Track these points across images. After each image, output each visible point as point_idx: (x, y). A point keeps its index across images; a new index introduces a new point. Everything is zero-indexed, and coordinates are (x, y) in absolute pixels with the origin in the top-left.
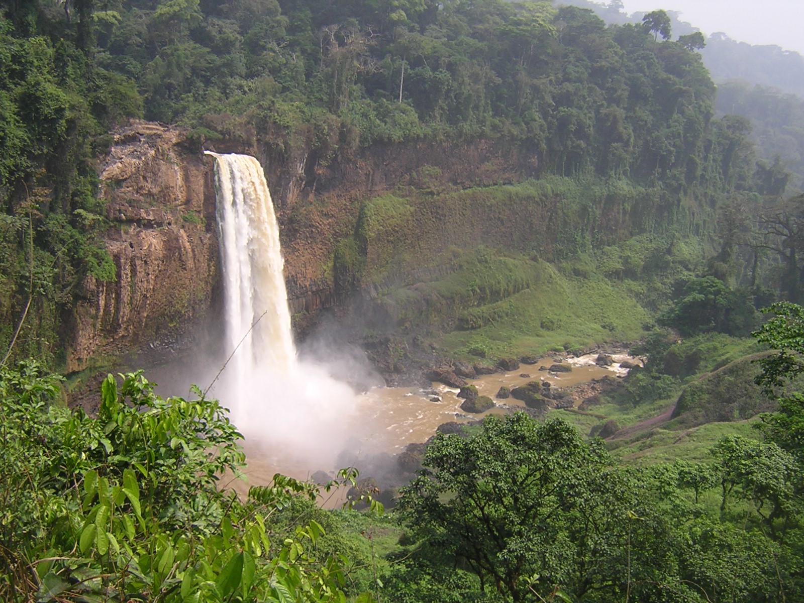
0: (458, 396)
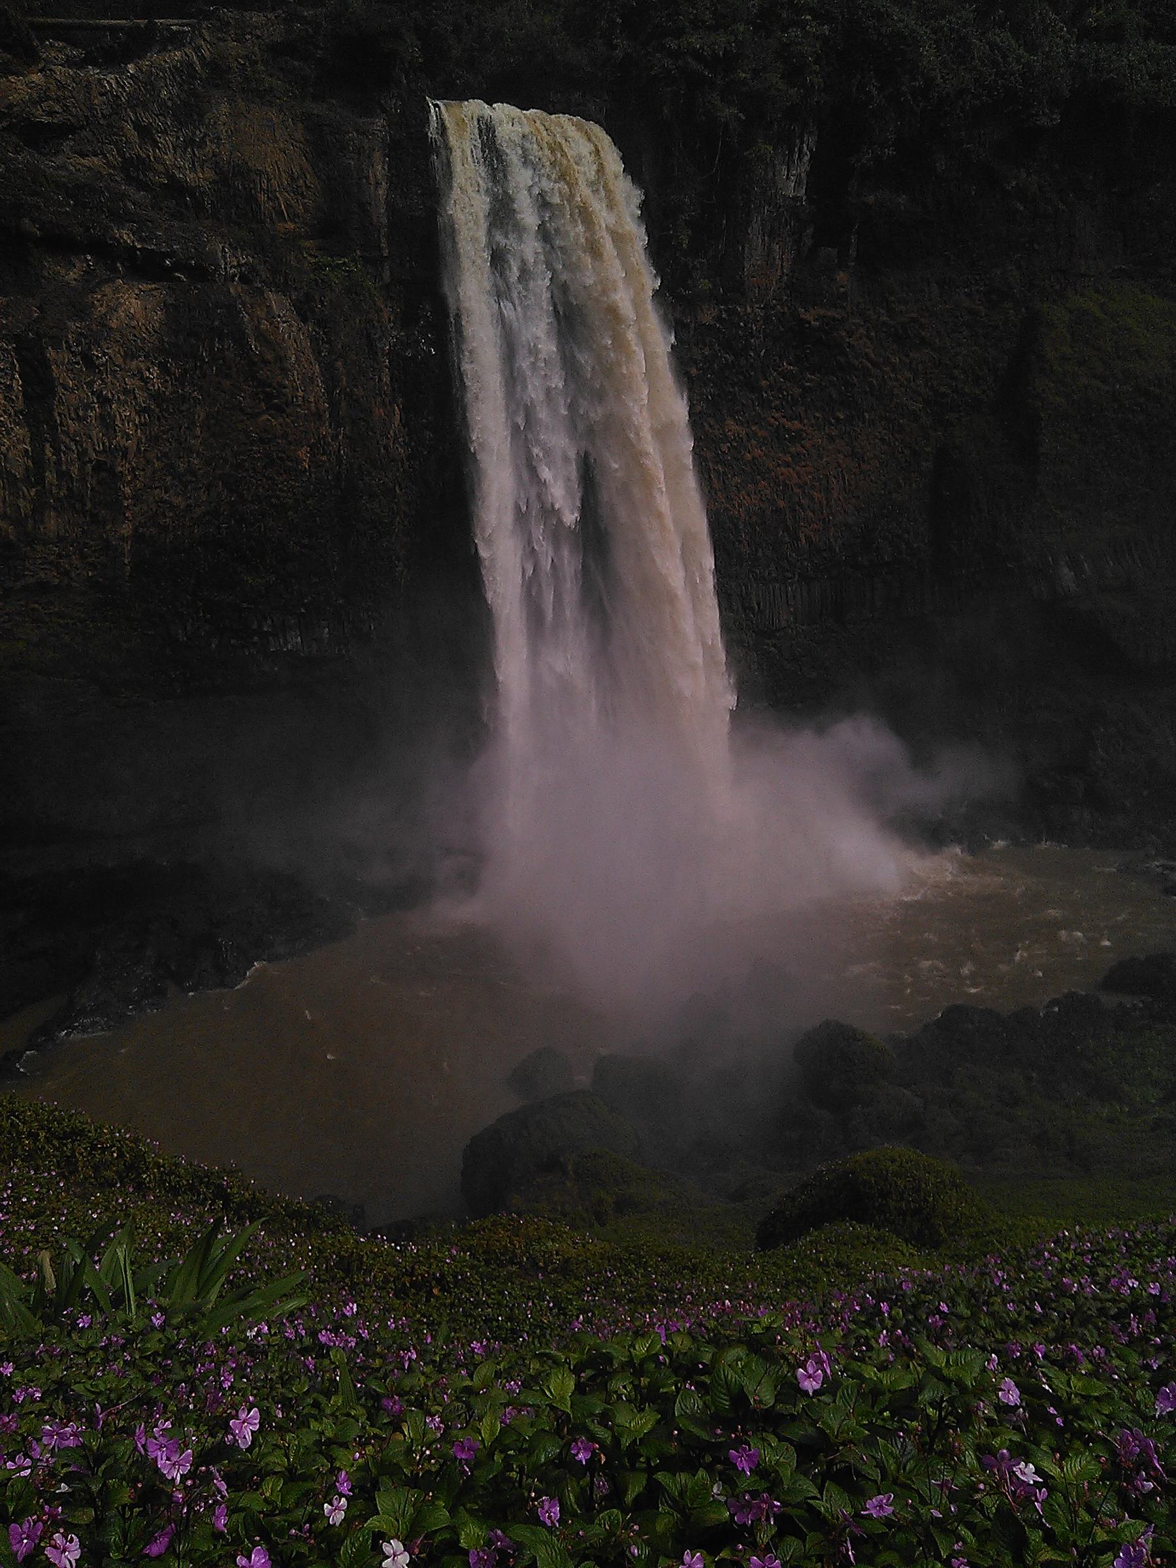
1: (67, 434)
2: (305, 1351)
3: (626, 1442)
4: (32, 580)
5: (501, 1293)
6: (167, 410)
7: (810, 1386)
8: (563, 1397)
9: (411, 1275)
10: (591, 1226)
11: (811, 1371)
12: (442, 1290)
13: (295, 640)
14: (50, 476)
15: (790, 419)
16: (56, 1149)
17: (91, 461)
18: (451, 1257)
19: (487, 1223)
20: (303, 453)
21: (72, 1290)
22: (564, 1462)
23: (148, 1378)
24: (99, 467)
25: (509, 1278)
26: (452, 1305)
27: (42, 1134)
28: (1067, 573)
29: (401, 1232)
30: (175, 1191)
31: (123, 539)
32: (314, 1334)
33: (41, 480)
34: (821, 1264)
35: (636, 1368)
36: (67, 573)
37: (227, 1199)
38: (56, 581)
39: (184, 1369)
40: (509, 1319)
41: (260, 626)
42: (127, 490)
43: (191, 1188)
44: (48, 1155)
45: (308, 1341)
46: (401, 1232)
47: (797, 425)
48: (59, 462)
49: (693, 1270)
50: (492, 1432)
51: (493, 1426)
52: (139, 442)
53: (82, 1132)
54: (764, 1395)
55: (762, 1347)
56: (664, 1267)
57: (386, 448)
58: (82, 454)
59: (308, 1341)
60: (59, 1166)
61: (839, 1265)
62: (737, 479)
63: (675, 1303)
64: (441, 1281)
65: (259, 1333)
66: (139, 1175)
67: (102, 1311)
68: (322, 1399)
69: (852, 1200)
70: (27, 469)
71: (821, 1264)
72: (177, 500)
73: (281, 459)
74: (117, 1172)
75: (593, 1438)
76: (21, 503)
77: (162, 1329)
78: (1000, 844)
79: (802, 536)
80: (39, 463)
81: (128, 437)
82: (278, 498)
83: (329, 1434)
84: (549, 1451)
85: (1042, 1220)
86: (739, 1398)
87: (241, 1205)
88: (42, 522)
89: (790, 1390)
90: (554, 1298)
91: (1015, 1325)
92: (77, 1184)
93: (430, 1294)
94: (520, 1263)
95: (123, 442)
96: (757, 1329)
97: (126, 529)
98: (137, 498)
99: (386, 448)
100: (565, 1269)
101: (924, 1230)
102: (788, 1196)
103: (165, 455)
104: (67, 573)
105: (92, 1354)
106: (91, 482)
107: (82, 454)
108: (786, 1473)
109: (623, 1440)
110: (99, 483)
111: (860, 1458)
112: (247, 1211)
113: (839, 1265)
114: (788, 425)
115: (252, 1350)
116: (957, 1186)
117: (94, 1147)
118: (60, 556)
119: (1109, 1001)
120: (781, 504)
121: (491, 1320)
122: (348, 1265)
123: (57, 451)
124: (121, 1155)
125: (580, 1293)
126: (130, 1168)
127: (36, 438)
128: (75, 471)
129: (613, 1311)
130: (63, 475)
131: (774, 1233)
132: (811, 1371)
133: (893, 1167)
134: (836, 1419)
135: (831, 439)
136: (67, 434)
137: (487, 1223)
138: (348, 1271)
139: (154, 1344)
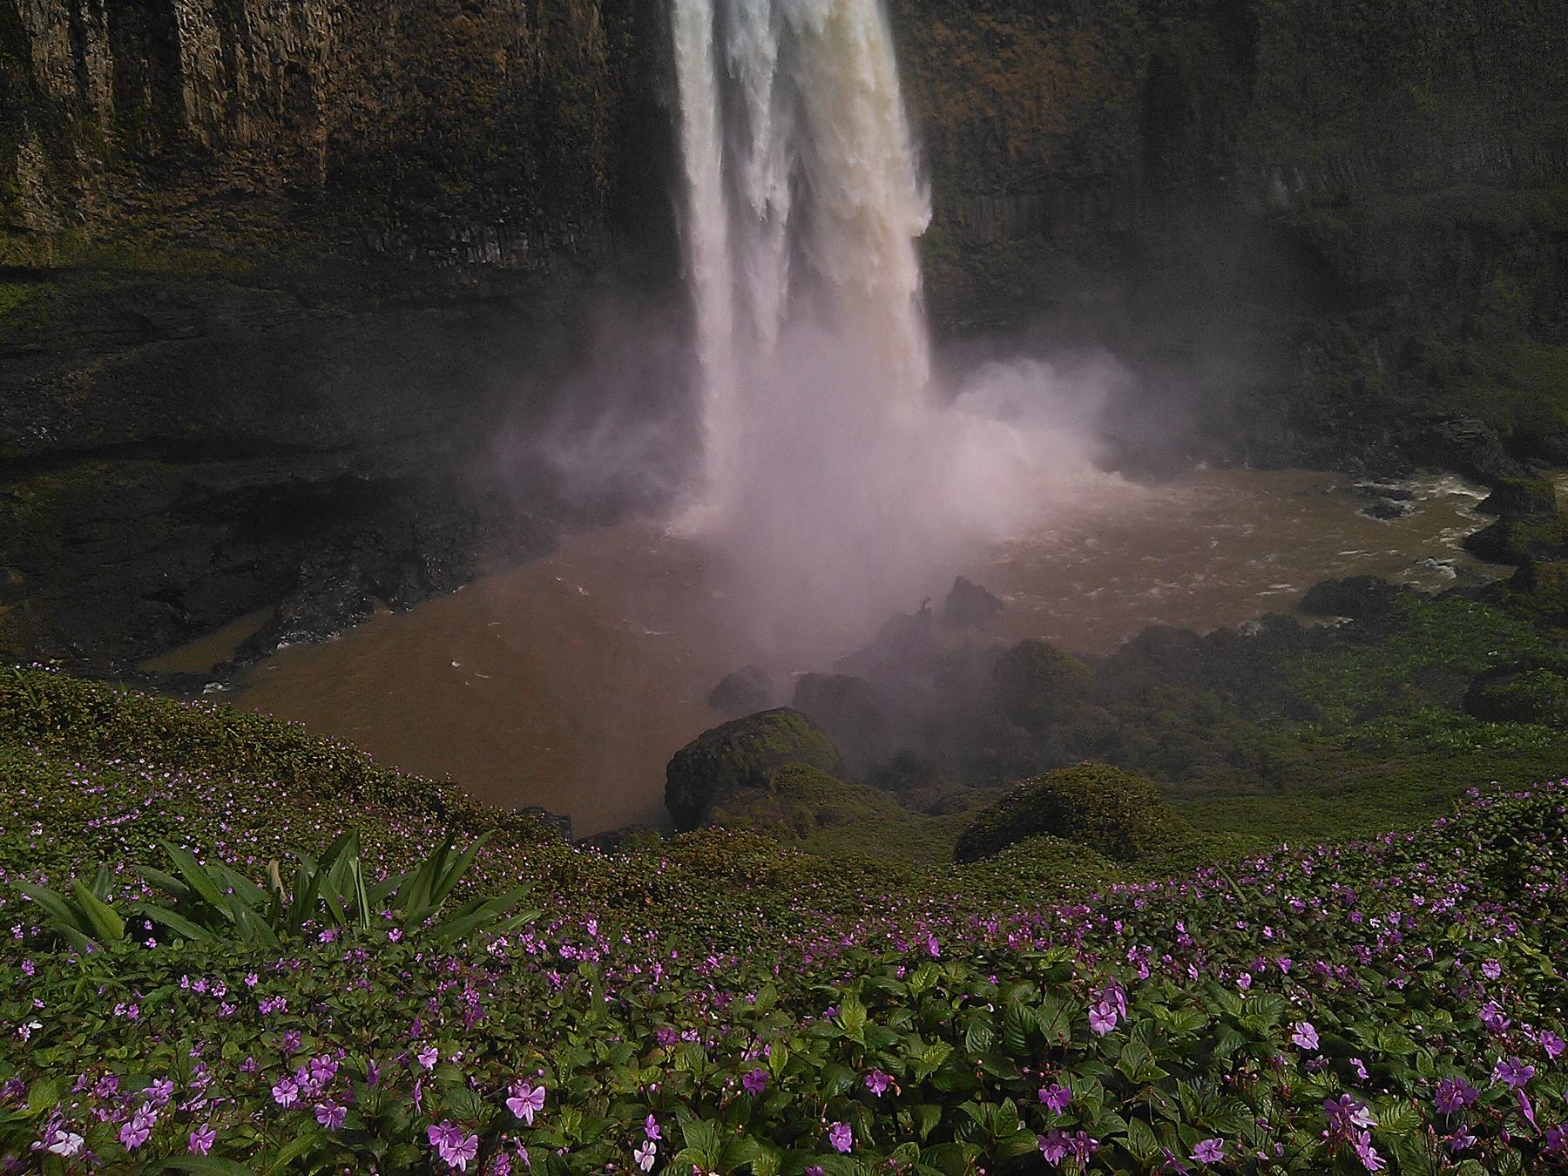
0: (1482, 508)
1: (257, 33)
2: (547, 965)
3: (920, 1076)
4: (227, 187)
5: (712, 903)
6: (359, 10)
7: (1101, 1027)
8: (855, 1030)
9: (625, 885)
10: (793, 837)
11: (1103, 1012)
12: (655, 900)
13: (494, 252)
14: (242, 78)
15: (1001, 23)
16: (273, 760)
17: (283, 63)
18: (662, 869)
19: (695, 836)
20: (500, 56)
21: (307, 902)
22: (857, 1093)
23: (391, 989)
24: (291, 69)
25: (721, 889)
26: (665, 915)
27: (259, 746)
28: (1280, 188)
29: (609, 842)
30: (390, 801)
31: (317, 144)
32: (554, 949)
33: (232, 83)
34: (1021, 877)
35: (914, 1003)
36: (261, 180)
37: (441, 810)
38: (251, 189)
39: (427, 984)
40: (721, 928)
41: (459, 237)
42: (321, 94)
43: (406, 799)
44: (265, 766)
45: (547, 956)
46: (609, 842)
47: (1008, 29)
48: (250, 64)
49: (898, 882)
50: (780, 1063)
51: (781, 1056)
52: (332, 42)
53: (298, 745)
54: (1058, 1031)
55: (1053, 982)
56: (869, 879)
57: (584, 50)
58: (274, 55)
59: (547, 956)
60: (276, 778)
61: (1040, 878)
62: (945, 87)
63: (880, 913)
64: (653, 891)
65: (500, 946)
66: (354, 786)
67: (335, 921)
68: (575, 1013)
69: (1049, 814)
70: (219, 71)
71: (1021, 877)
72: (372, 105)
73: (477, 62)
74: (333, 783)
75: (887, 1070)
76: (214, 106)
77: (400, 942)
78: (1203, 466)
79: (1011, 147)
80: (230, 64)
81: (321, 38)
82: (474, 103)
83: (603, 1056)
84: (843, 1081)
85: (1238, 836)
86: (1035, 1037)
87: (455, 817)
88: (236, 127)
89: (1080, 1028)
90: (764, 910)
91: (1246, 945)
92: (296, 795)
93: (643, 904)
94: (728, 874)
95: (315, 43)
96: (1043, 965)
97: (321, 135)
98: (330, 101)
99: (584, 50)
100: (772, 880)
101: (1122, 849)
102: (986, 811)
103: (359, 56)
104: (261, 180)
105: (336, 968)
106: (285, 84)
107: (274, 55)
108: (1095, 1109)
109: (918, 1074)
110: (293, 86)
111: (1156, 1098)
112: (466, 822)
113: (1040, 878)
114: (999, 28)
115: (492, 964)
116: (1154, 803)
117: (310, 759)
118: (253, 162)
119: (1308, 623)
120: (991, 113)
121: (703, 929)
122: (563, 876)
123: (248, 52)
124: (337, 766)
125: (788, 903)
126: (346, 779)
127: (227, 39)
128: (267, 74)
129: (822, 921)
130: (253, 77)
131: (971, 849)
132: (1103, 1012)
133: (1093, 784)
134: (1135, 1059)
135: (1043, 44)
136: (257, 33)
137: (695, 836)
138: (562, 882)
139: (395, 957)
